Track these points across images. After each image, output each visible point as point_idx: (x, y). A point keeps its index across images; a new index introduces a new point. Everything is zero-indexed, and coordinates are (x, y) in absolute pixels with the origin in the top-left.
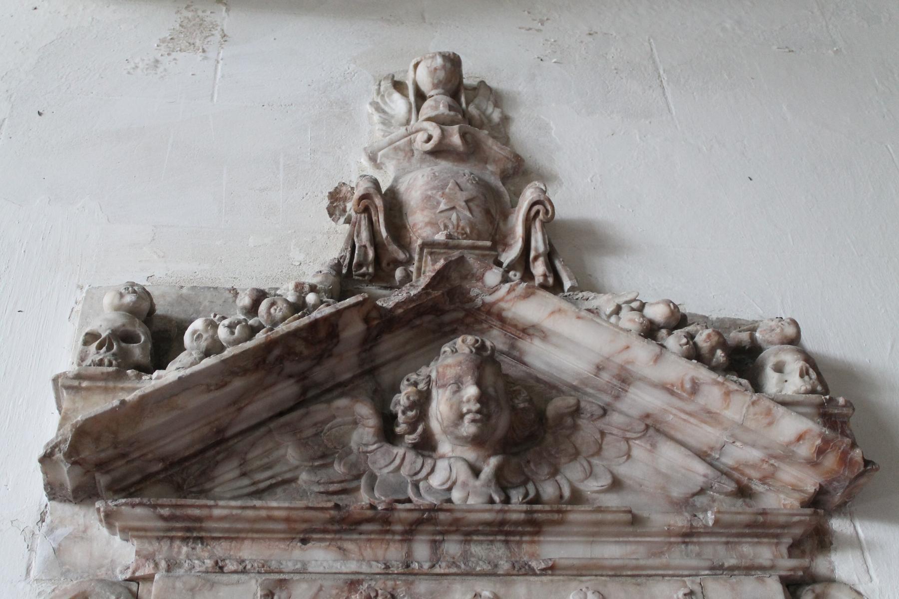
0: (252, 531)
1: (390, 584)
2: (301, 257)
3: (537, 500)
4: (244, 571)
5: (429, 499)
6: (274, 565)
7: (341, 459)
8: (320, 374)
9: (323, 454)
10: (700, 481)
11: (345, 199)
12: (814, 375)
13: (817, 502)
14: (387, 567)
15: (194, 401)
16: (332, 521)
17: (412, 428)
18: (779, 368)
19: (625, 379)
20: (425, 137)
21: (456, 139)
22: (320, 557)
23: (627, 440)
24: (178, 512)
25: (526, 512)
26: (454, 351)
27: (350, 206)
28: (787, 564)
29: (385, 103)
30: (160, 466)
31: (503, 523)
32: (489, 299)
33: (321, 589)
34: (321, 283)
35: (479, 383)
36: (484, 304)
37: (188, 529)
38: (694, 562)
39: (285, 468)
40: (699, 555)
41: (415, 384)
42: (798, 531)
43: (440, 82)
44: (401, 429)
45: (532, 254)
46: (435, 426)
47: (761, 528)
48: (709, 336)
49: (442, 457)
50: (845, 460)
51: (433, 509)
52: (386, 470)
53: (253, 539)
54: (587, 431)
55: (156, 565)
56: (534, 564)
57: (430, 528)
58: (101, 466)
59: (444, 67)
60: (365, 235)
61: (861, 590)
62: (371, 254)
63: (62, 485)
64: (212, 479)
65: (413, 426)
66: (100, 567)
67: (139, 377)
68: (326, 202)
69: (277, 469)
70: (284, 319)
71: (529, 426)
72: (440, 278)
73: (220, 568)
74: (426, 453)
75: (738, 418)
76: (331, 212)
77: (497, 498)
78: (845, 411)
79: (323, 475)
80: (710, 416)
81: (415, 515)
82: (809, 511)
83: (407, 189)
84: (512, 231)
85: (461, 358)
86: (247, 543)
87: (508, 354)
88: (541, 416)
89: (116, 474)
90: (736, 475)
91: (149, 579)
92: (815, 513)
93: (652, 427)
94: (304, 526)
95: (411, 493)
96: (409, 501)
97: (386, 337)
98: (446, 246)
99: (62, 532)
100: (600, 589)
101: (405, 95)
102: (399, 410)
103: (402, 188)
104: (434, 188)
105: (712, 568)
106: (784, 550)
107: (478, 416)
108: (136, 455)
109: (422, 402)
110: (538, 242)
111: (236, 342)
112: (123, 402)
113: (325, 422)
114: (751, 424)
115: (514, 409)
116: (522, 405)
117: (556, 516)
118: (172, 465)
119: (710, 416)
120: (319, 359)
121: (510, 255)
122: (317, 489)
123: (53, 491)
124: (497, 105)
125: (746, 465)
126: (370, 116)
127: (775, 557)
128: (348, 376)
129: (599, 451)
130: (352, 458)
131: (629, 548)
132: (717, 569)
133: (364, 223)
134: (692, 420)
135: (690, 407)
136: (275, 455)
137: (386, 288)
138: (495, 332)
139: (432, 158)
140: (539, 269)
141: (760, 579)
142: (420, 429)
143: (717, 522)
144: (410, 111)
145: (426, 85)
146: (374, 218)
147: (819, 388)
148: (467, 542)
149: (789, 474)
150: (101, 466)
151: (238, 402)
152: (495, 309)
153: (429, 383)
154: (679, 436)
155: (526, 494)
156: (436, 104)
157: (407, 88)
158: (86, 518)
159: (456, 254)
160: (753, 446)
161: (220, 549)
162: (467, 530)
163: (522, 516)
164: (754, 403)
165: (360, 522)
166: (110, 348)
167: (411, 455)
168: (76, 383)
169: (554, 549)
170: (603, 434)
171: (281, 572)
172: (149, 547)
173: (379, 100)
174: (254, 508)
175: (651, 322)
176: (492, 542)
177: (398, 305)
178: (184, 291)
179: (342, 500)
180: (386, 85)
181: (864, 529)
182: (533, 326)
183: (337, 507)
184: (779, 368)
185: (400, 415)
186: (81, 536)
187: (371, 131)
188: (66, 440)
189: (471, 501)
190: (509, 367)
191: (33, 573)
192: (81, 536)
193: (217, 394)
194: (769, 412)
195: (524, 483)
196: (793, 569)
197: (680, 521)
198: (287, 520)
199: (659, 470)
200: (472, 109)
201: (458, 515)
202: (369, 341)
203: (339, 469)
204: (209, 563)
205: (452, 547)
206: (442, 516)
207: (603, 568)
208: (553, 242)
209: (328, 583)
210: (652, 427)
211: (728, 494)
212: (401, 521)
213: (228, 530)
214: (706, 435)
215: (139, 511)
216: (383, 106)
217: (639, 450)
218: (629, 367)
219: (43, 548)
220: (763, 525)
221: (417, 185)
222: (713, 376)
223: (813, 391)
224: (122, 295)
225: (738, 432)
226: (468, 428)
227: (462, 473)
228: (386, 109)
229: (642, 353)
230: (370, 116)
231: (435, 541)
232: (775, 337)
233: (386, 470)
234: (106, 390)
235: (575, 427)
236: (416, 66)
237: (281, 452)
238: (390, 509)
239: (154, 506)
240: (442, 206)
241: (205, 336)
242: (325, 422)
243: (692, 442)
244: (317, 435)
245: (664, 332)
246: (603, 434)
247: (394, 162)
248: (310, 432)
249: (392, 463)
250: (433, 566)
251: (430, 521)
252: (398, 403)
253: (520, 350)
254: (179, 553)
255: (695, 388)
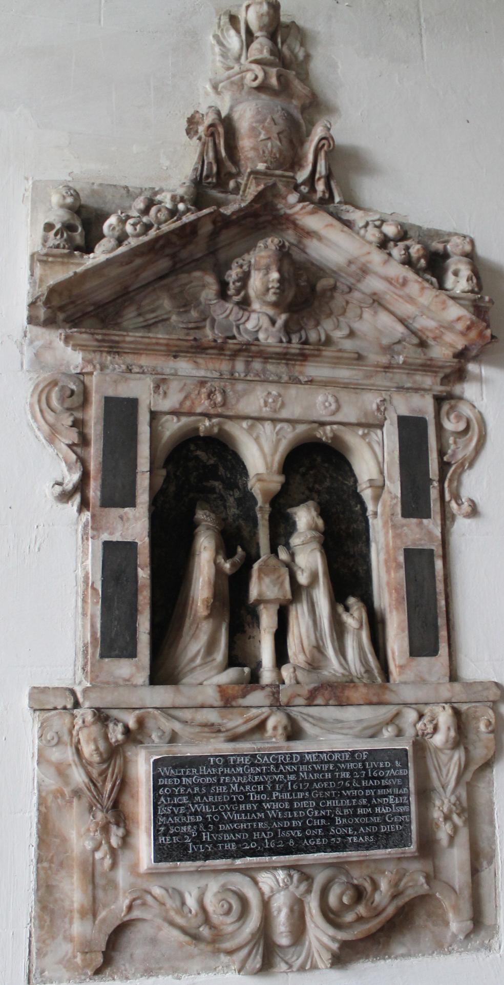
0: (145, 350)
1: (222, 384)
2: (167, 163)
3: (306, 342)
4: (143, 373)
5: (246, 338)
6: (159, 370)
7: (195, 307)
8: (184, 254)
9: (185, 303)
10: (399, 336)
11: (198, 123)
12: (475, 281)
13: (462, 355)
14: (221, 375)
15: (115, 272)
16: (192, 347)
17: (238, 292)
18: (456, 273)
19: (365, 271)
20: (253, 77)
21: (274, 81)
22: (184, 366)
23: (361, 308)
24: (106, 338)
25: (300, 349)
26: (266, 247)
27: (201, 129)
28: (439, 389)
29: (224, 37)
30: (92, 308)
31: (286, 354)
32: (289, 212)
33: (185, 385)
34: (186, 193)
35: (280, 271)
36: (285, 214)
37: (111, 347)
38: (388, 384)
39: (163, 312)
40: (392, 379)
41: (241, 266)
42: (448, 371)
43: (265, 25)
44: (231, 292)
45: (317, 176)
46: (252, 293)
47: (428, 367)
48: (418, 250)
49: (254, 311)
50: (481, 335)
51: (248, 344)
52: (221, 317)
53: (147, 354)
54: (339, 300)
55: (94, 366)
56: (301, 378)
57: (246, 354)
58: (61, 308)
59: (268, 13)
60: (211, 154)
61: (476, 404)
62: (215, 169)
63: (37, 318)
64: (121, 317)
65: (238, 292)
66: (61, 365)
67: (82, 256)
68: (185, 125)
69: (158, 313)
70: (166, 221)
71: (306, 294)
72: (260, 196)
73: (129, 370)
74: (244, 307)
75: (426, 303)
76: (188, 133)
77: (284, 340)
78: (488, 305)
79: (185, 318)
80: (411, 300)
81: (238, 347)
82: (456, 360)
83: (239, 119)
84: (306, 156)
85: (270, 253)
86: (143, 357)
87: (296, 246)
88: (313, 288)
89: (69, 313)
90: (420, 334)
91: (91, 374)
92: (460, 362)
93: (377, 301)
94: (176, 349)
95: (235, 332)
96: (234, 337)
97: (224, 231)
98: (265, 174)
99: (38, 343)
100: (336, 394)
101: (238, 31)
102: (231, 280)
103: (236, 116)
104: (257, 122)
105: (397, 388)
106: (438, 380)
107: (278, 291)
108: (79, 302)
109: (245, 278)
110: (322, 168)
111: (138, 236)
112: (75, 273)
113: (186, 284)
114: (433, 308)
115: (298, 285)
116: (303, 284)
117: (316, 353)
118: (99, 307)
119: (411, 300)
120: (184, 246)
121: (303, 175)
122: (181, 326)
123: (31, 320)
124: (302, 44)
125: (427, 329)
126: (212, 46)
127: (433, 384)
128: (199, 255)
129: (344, 313)
130: (202, 307)
131: (354, 372)
132: (401, 389)
133: (211, 144)
134: (400, 300)
135: (401, 293)
136: (157, 303)
137: (223, 192)
138: (290, 232)
139: (256, 92)
140: (320, 187)
141: (423, 396)
142: (242, 294)
143: (404, 362)
144: (242, 49)
145: (254, 26)
146: (217, 141)
147: (476, 289)
148: (265, 363)
149: (449, 337)
150: (61, 308)
151: (137, 272)
152: (292, 218)
153: (250, 266)
154: (391, 308)
155: (301, 338)
156: (261, 47)
157: (239, 22)
158: (55, 337)
159: (270, 181)
160: (433, 319)
161: (129, 359)
162: (265, 356)
163: (298, 351)
164: (437, 296)
165: (207, 349)
166: (62, 236)
167: (236, 309)
168: (45, 258)
169: (313, 370)
170: (347, 302)
171: (163, 374)
172: (90, 356)
173: (219, 34)
174: (149, 337)
175: (385, 236)
176: (279, 364)
177: (233, 213)
178: (95, 187)
179: (198, 334)
180: (225, 20)
181: (486, 371)
182: (314, 232)
183: (195, 339)
184: (456, 273)
185: (231, 284)
186: (49, 346)
187: (213, 63)
188: (43, 295)
189: (270, 341)
190: (297, 255)
191: (25, 367)
192: (49, 346)
193: (127, 267)
194: (444, 302)
195: (299, 331)
196: (441, 392)
197: (384, 360)
198: (167, 345)
199: (379, 326)
200: (285, 50)
201: (262, 348)
202: (214, 234)
203: (194, 314)
204: (124, 367)
205: (257, 365)
206: (253, 348)
207: (339, 383)
208: (333, 169)
209: (188, 382)
210: (377, 301)
211: (413, 345)
212: (230, 349)
213: (131, 349)
214: (406, 309)
215: (84, 336)
216: (222, 39)
217: (367, 314)
218: (368, 265)
219: (28, 353)
220: (429, 366)
221: (246, 116)
222: (416, 277)
223: (472, 291)
224: (64, 197)
225: (425, 311)
226: (271, 297)
227: (265, 322)
228: (225, 43)
229: (377, 257)
230: (212, 46)
231: (247, 361)
232: (458, 250)
233: (221, 317)
234: (63, 263)
235: (332, 297)
236: (248, 7)
237: (161, 302)
238: (225, 342)
239: (93, 334)
240: (262, 137)
241: (117, 228)
242: (186, 284)
243: (399, 313)
244: (181, 292)
245: (392, 243)
246: (347, 302)
247: (230, 93)
248: (176, 290)
249: (225, 312)
250: (246, 376)
251: (247, 350)
252: (231, 276)
253: (304, 245)
254: (106, 360)
255: (405, 283)
